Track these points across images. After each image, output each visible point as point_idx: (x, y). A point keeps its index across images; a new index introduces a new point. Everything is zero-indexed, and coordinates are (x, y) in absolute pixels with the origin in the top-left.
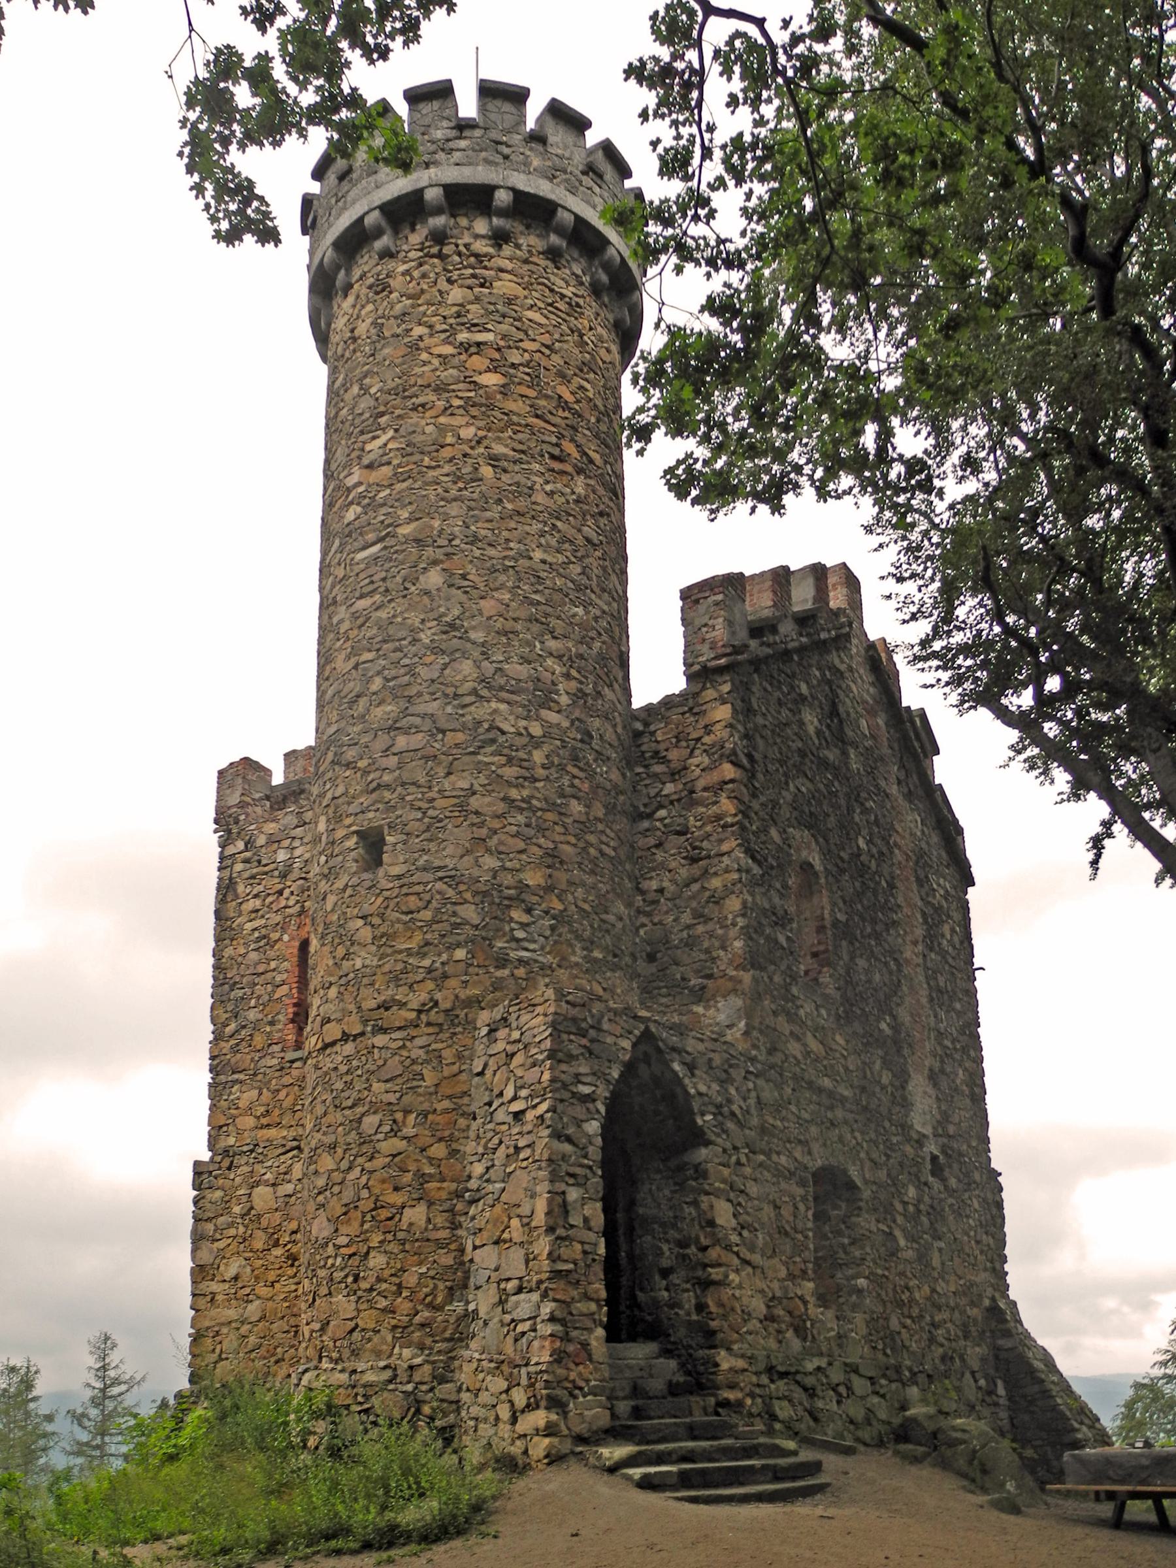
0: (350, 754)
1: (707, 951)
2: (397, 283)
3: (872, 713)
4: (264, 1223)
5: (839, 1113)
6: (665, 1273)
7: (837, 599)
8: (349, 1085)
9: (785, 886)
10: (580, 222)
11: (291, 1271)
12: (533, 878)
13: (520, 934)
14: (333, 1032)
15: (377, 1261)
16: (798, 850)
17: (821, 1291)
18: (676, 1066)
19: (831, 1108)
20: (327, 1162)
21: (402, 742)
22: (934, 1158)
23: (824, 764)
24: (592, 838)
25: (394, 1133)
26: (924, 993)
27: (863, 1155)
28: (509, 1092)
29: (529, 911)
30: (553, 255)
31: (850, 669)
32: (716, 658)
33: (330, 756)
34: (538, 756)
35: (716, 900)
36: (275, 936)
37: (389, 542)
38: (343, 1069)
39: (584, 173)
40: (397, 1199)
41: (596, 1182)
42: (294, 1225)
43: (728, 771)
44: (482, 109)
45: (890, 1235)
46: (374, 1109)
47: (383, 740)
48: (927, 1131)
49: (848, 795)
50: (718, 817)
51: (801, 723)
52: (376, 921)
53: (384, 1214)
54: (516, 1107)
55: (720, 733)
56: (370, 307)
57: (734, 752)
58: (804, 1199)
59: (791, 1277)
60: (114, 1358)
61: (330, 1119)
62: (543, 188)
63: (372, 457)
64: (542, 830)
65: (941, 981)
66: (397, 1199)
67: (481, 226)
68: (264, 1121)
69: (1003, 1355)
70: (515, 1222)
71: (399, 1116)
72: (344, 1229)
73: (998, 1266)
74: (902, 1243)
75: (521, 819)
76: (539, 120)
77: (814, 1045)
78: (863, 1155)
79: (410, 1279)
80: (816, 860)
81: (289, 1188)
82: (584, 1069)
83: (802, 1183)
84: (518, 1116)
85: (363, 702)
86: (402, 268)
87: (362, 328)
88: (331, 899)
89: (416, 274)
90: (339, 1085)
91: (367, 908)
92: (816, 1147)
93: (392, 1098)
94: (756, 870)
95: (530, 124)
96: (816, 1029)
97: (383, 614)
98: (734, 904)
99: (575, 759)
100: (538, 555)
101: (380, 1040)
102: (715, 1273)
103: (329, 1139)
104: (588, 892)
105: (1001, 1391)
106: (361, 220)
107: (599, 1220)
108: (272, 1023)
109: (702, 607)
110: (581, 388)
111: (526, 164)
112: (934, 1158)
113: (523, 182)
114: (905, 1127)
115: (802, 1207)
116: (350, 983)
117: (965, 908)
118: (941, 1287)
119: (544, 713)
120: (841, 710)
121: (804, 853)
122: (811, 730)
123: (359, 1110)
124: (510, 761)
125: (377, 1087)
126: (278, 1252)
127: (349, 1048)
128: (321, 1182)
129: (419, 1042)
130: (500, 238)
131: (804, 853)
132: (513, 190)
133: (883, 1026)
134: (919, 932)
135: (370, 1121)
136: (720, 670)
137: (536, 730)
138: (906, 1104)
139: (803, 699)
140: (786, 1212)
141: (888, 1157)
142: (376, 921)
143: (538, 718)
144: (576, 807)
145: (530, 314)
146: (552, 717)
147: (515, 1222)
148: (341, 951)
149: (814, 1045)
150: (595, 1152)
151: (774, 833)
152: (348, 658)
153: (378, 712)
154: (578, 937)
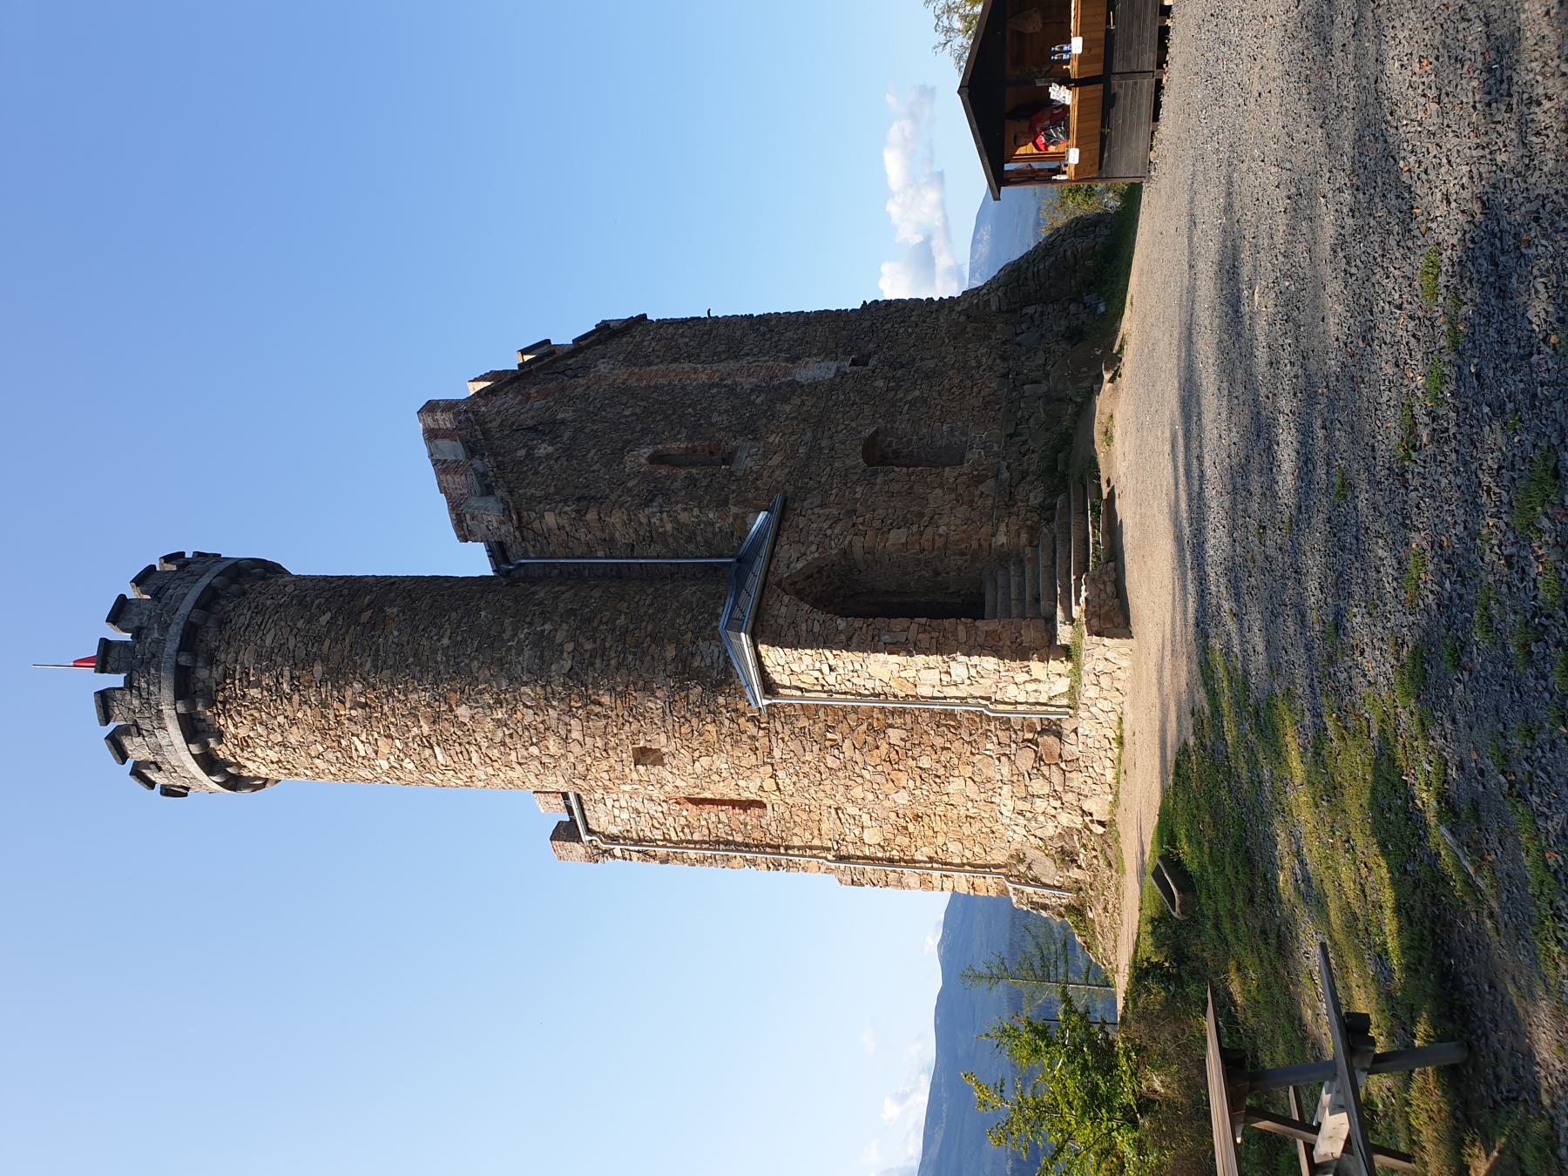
0: (581, 768)
1: (714, 534)
2: (242, 732)
3: (528, 397)
4: (890, 836)
5: (824, 443)
6: (936, 573)
7: (444, 420)
8: (806, 775)
9: (667, 477)
10: (198, 605)
11: (926, 819)
12: (671, 652)
13: (708, 660)
14: (769, 784)
15: (925, 762)
16: (640, 465)
17: (966, 648)
18: (800, 565)
19: (821, 449)
20: (857, 792)
21: (575, 735)
22: (854, 363)
23: (573, 439)
24: (642, 611)
25: (838, 747)
26: (733, 364)
27: (853, 425)
28: (817, 674)
29: (693, 655)
30: (222, 624)
31: (499, 412)
32: (511, 520)
33: (578, 782)
34: (588, 646)
35: (679, 527)
36: (683, 821)
37: (433, 740)
38: (794, 778)
39: (159, 600)
40: (884, 747)
41: (880, 622)
42: (893, 815)
43: (591, 516)
44: (116, 671)
45: (912, 403)
46: (822, 760)
47: (576, 748)
48: (834, 365)
49: (594, 422)
50: (624, 524)
51: (548, 456)
52: (697, 754)
53: (893, 756)
54: (826, 669)
55: (564, 521)
56: (258, 751)
57: (578, 511)
58: (886, 474)
59: (941, 485)
60: (981, 968)
61: (828, 788)
62: (175, 630)
63: (370, 751)
64: (638, 644)
65: (721, 348)
66: (884, 747)
67: (203, 673)
68: (816, 833)
69: (1004, 308)
70: (903, 674)
71: (828, 744)
72: (903, 783)
73: (935, 307)
74: (917, 393)
75: (630, 657)
76: (125, 631)
77: (776, 460)
78: (853, 425)
79: (939, 742)
80: (646, 451)
81: (865, 817)
82: (804, 627)
83: (875, 474)
84: (831, 669)
85: (545, 760)
86: (232, 728)
87: (273, 755)
88: (679, 783)
89: (237, 719)
90: (806, 781)
91: (688, 759)
92: (850, 462)
93: (816, 748)
94: (659, 499)
95: (127, 637)
96: (764, 456)
97: (484, 744)
98: (684, 517)
99: (590, 621)
100: (445, 641)
101: (777, 753)
102: (940, 542)
103: (841, 789)
104: (679, 615)
105: (1030, 310)
106: (194, 756)
107: (904, 622)
108: (746, 825)
109: (475, 529)
110: (318, 606)
111: (158, 642)
112: (854, 363)
113: (172, 646)
114: (832, 387)
115: (892, 476)
116: (736, 771)
117: (662, 323)
118: (950, 359)
119: (558, 640)
120: (531, 423)
121: (643, 461)
122: (550, 449)
123: (822, 768)
124: (592, 664)
125: (808, 757)
126: (911, 827)
127: (781, 774)
128: (870, 796)
129: (779, 728)
130: (211, 661)
131: (643, 461)
132: (178, 651)
133: (758, 401)
134: (686, 366)
135: (830, 761)
136: (520, 518)
137: (569, 647)
138: (814, 385)
139: (528, 455)
140: (895, 487)
141: (854, 403)
142: (697, 754)
143: (561, 645)
144: (621, 621)
145: (268, 642)
146: (560, 637)
147: (903, 674)
148: (715, 777)
149: (776, 460)
150: (858, 623)
151: (630, 484)
152: (513, 769)
153: (553, 749)
154: (709, 623)
